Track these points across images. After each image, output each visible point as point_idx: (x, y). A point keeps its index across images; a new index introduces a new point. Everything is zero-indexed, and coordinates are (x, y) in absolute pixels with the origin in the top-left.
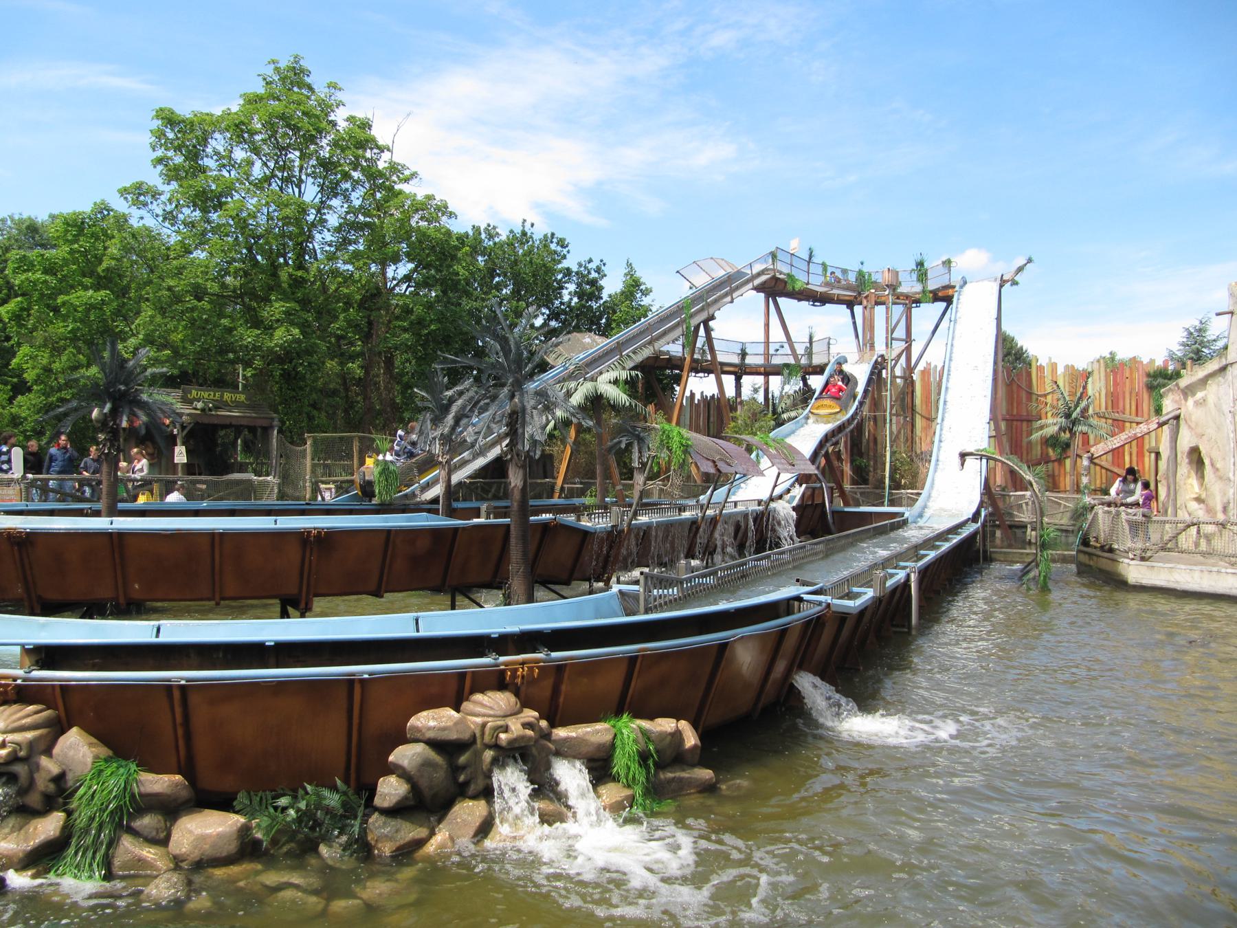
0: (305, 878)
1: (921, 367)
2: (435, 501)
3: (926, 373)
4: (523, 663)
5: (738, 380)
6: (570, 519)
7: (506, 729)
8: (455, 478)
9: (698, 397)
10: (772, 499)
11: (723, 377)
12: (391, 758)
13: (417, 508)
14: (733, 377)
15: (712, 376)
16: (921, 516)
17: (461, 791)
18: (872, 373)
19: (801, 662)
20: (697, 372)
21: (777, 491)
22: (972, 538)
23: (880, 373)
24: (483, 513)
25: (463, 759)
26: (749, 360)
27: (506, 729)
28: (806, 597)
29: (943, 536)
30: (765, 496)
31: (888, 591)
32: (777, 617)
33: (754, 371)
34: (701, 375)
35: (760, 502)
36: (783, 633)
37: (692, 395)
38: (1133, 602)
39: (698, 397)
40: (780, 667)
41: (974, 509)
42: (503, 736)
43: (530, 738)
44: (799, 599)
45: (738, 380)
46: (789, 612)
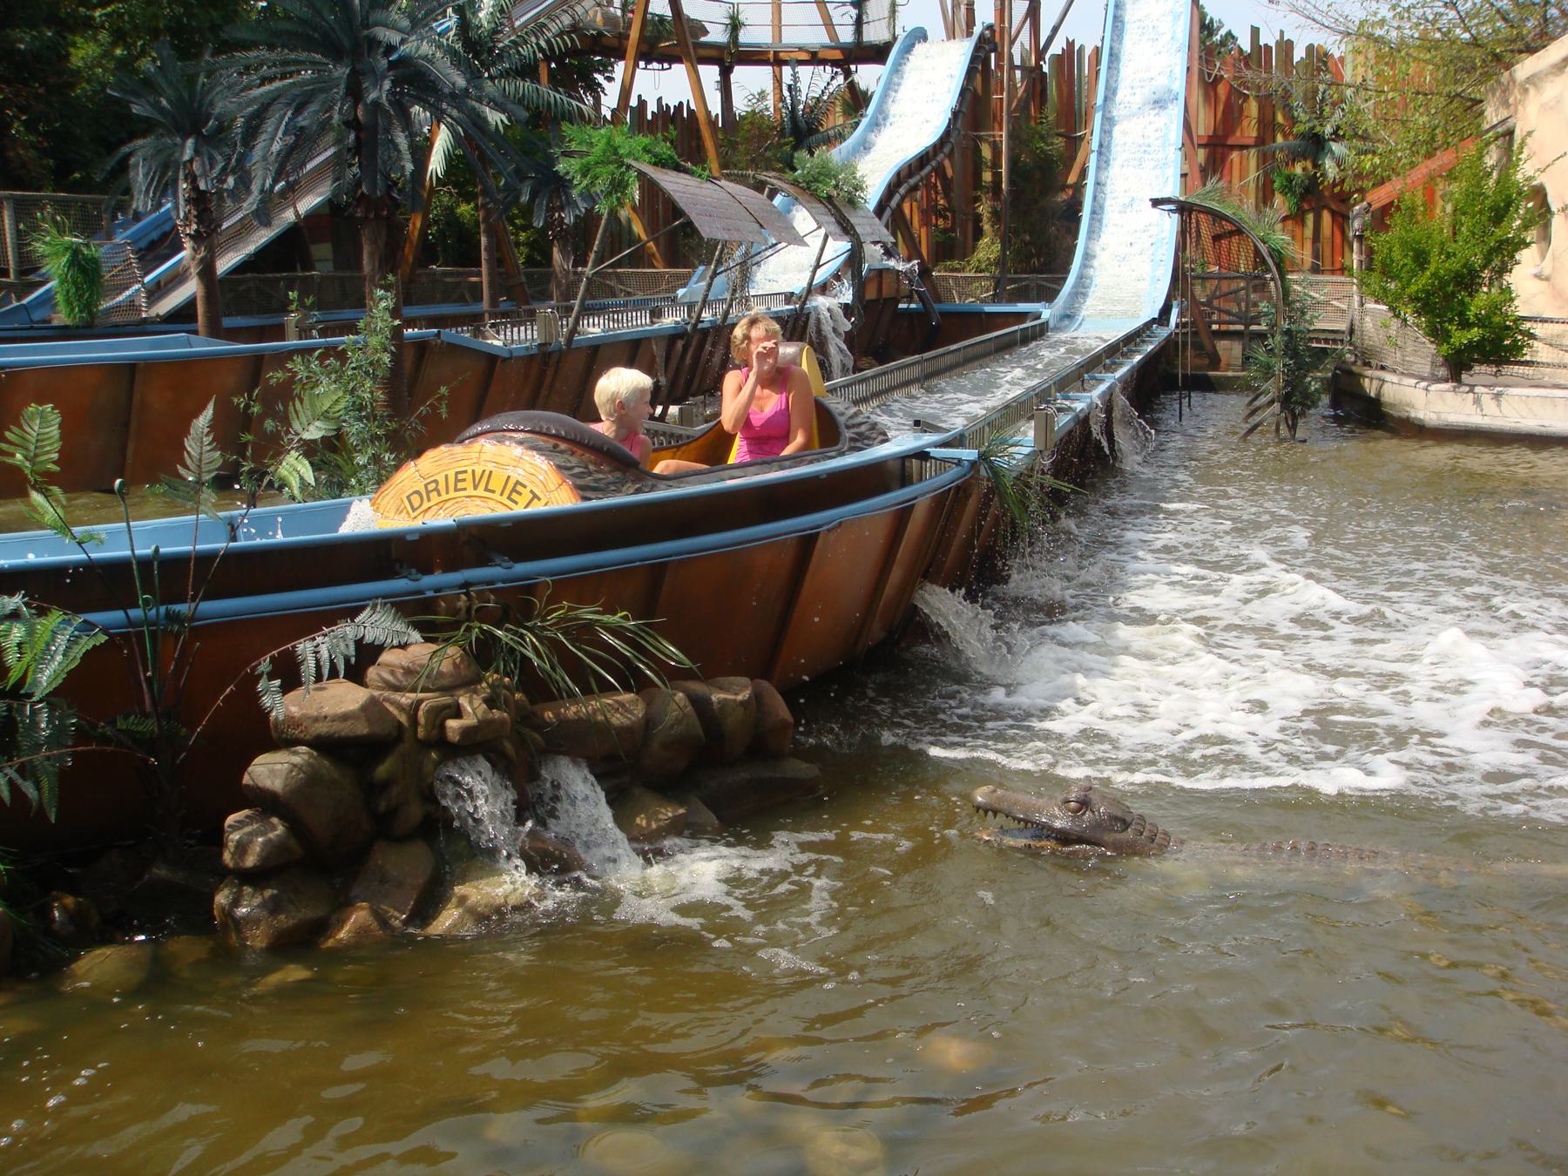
0: (310, 968)
1: (1057, 48)
2: (190, 304)
3: (1058, 60)
4: (466, 585)
5: (726, 74)
6: (464, 335)
7: (458, 713)
8: (224, 264)
9: (652, 107)
10: (810, 290)
11: (701, 68)
12: (246, 780)
13: (142, 328)
14: (715, 70)
15: (679, 69)
16: (1068, 317)
17: (385, 828)
18: (974, 59)
19: (930, 569)
20: (648, 62)
21: (822, 275)
22: (1168, 349)
23: (986, 61)
24: (291, 329)
25: (382, 771)
26: (745, 37)
27: (458, 713)
28: (934, 452)
29: (1114, 352)
30: (798, 284)
31: (1057, 438)
32: (887, 490)
33: (754, 57)
34: (655, 65)
35: (789, 297)
36: (903, 515)
37: (642, 103)
38: (1391, 451)
39: (652, 107)
40: (896, 575)
41: (1160, 303)
42: (452, 724)
43: (502, 722)
44: (922, 455)
45: (726, 74)
46: (905, 480)
